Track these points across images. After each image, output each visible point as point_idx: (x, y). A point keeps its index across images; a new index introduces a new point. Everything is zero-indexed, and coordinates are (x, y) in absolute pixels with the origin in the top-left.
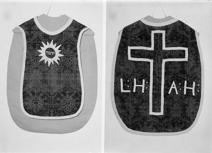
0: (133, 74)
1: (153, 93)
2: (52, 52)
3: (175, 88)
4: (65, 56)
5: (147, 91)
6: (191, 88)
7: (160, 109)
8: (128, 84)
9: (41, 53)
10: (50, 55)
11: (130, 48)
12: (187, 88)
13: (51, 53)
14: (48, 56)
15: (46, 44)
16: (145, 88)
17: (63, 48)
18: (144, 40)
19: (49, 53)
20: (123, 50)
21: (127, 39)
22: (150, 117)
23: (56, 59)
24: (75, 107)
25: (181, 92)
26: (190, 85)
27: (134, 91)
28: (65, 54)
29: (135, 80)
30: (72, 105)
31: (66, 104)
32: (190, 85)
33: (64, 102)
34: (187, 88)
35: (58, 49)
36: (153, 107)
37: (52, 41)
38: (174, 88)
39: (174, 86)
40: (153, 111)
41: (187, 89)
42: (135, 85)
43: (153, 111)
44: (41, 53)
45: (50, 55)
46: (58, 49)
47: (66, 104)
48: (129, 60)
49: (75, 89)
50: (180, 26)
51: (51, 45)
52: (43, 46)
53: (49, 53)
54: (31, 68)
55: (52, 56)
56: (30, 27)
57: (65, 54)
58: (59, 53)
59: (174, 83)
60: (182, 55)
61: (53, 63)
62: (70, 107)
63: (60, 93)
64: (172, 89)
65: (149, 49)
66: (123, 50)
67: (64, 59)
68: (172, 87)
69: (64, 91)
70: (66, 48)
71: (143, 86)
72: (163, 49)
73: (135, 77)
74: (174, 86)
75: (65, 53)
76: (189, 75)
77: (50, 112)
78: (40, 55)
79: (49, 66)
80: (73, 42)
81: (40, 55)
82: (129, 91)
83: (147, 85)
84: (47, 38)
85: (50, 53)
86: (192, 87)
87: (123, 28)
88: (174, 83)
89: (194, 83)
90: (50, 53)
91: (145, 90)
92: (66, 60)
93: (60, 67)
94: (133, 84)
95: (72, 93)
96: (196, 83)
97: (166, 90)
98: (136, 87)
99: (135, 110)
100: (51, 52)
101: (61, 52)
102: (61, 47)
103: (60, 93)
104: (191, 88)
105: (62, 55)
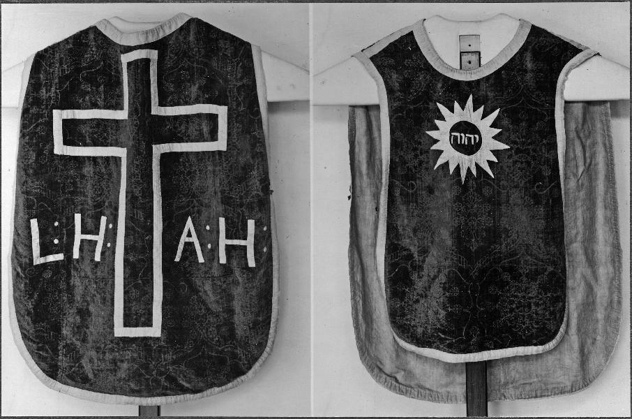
0: (73, 200)
1: (126, 261)
2: (472, 136)
3: (194, 239)
4: (511, 148)
5: (109, 253)
6: (242, 243)
7: (150, 314)
8: (57, 232)
9: (436, 141)
10: (466, 143)
11: (59, 116)
12: (230, 242)
13: (469, 139)
14: (458, 146)
15: (452, 110)
16: (105, 245)
17: (505, 122)
18: (102, 88)
19: (461, 137)
20: (37, 126)
21: (49, 87)
22: (118, 344)
23: (484, 157)
24: (549, 320)
25: (212, 255)
26: (236, 230)
27: (76, 255)
28: (515, 143)
29: (78, 217)
30: (537, 314)
31: (517, 308)
32: (236, 230)
33: (514, 301)
34: (230, 242)
35: (491, 126)
36: (125, 311)
37: (471, 97)
38: (191, 240)
39: (189, 235)
40: (125, 325)
41: (228, 248)
42: (79, 237)
43: (125, 325)
44: (436, 141)
45: (466, 143)
46: (491, 126)
47: (517, 308)
48: (58, 155)
49: (549, 259)
50: (202, 35)
51: (469, 113)
52: (442, 118)
53: (461, 137)
54: (412, 189)
55: (470, 149)
56: (400, 60)
57: (515, 143)
58: (494, 138)
59: (189, 224)
60: (73, 133)
61: (474, 172)
62: (530, 317)
63: (500, 270)
64: (185, 243)
65: (69, 114)
66: (37, 126)
67: (510, 157)
68: (184, 238)
69: (511, 262)
70: (516, 121)
71: (100, 238)
72: (153, 113)
73: (79, 208)
74: (189, 235)
75: (513, 137)
76: (232, 198)
77: (469, 337)
78: (434, 147)
79: (463, 179)
80: (536, 104)
81: (434, 147)
82: (60, 257)
83: (111, 235)
84: (457, 92)
85: (464, 138)
86: (245, 238)
87: (36, 52)
88: (189, 224)
89: (251, 224)
90: (464, 138)
91: (103, 253)
92: (517, 161)
93: (499, 186)
94: (71, 234)
95: (537, 273)
96: (258, 225)
97: (169, 249)
98: (82, 241)
99: (78, 317)
100: (467, 135)
101: (500, 134)
102: (498, 116)
103: (500, 270)
104: (242, 243)
105: (503, 146)
